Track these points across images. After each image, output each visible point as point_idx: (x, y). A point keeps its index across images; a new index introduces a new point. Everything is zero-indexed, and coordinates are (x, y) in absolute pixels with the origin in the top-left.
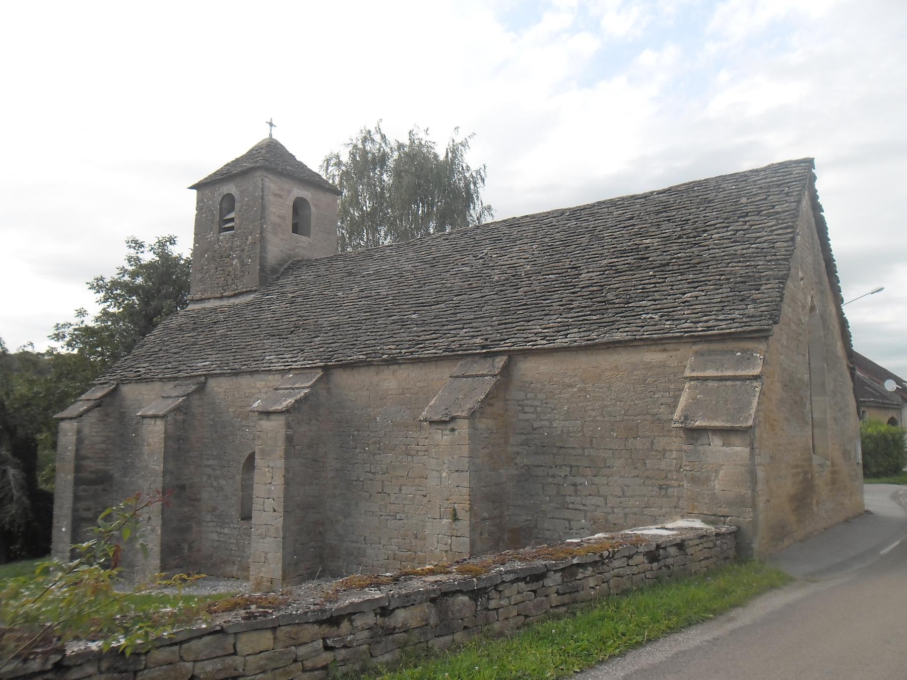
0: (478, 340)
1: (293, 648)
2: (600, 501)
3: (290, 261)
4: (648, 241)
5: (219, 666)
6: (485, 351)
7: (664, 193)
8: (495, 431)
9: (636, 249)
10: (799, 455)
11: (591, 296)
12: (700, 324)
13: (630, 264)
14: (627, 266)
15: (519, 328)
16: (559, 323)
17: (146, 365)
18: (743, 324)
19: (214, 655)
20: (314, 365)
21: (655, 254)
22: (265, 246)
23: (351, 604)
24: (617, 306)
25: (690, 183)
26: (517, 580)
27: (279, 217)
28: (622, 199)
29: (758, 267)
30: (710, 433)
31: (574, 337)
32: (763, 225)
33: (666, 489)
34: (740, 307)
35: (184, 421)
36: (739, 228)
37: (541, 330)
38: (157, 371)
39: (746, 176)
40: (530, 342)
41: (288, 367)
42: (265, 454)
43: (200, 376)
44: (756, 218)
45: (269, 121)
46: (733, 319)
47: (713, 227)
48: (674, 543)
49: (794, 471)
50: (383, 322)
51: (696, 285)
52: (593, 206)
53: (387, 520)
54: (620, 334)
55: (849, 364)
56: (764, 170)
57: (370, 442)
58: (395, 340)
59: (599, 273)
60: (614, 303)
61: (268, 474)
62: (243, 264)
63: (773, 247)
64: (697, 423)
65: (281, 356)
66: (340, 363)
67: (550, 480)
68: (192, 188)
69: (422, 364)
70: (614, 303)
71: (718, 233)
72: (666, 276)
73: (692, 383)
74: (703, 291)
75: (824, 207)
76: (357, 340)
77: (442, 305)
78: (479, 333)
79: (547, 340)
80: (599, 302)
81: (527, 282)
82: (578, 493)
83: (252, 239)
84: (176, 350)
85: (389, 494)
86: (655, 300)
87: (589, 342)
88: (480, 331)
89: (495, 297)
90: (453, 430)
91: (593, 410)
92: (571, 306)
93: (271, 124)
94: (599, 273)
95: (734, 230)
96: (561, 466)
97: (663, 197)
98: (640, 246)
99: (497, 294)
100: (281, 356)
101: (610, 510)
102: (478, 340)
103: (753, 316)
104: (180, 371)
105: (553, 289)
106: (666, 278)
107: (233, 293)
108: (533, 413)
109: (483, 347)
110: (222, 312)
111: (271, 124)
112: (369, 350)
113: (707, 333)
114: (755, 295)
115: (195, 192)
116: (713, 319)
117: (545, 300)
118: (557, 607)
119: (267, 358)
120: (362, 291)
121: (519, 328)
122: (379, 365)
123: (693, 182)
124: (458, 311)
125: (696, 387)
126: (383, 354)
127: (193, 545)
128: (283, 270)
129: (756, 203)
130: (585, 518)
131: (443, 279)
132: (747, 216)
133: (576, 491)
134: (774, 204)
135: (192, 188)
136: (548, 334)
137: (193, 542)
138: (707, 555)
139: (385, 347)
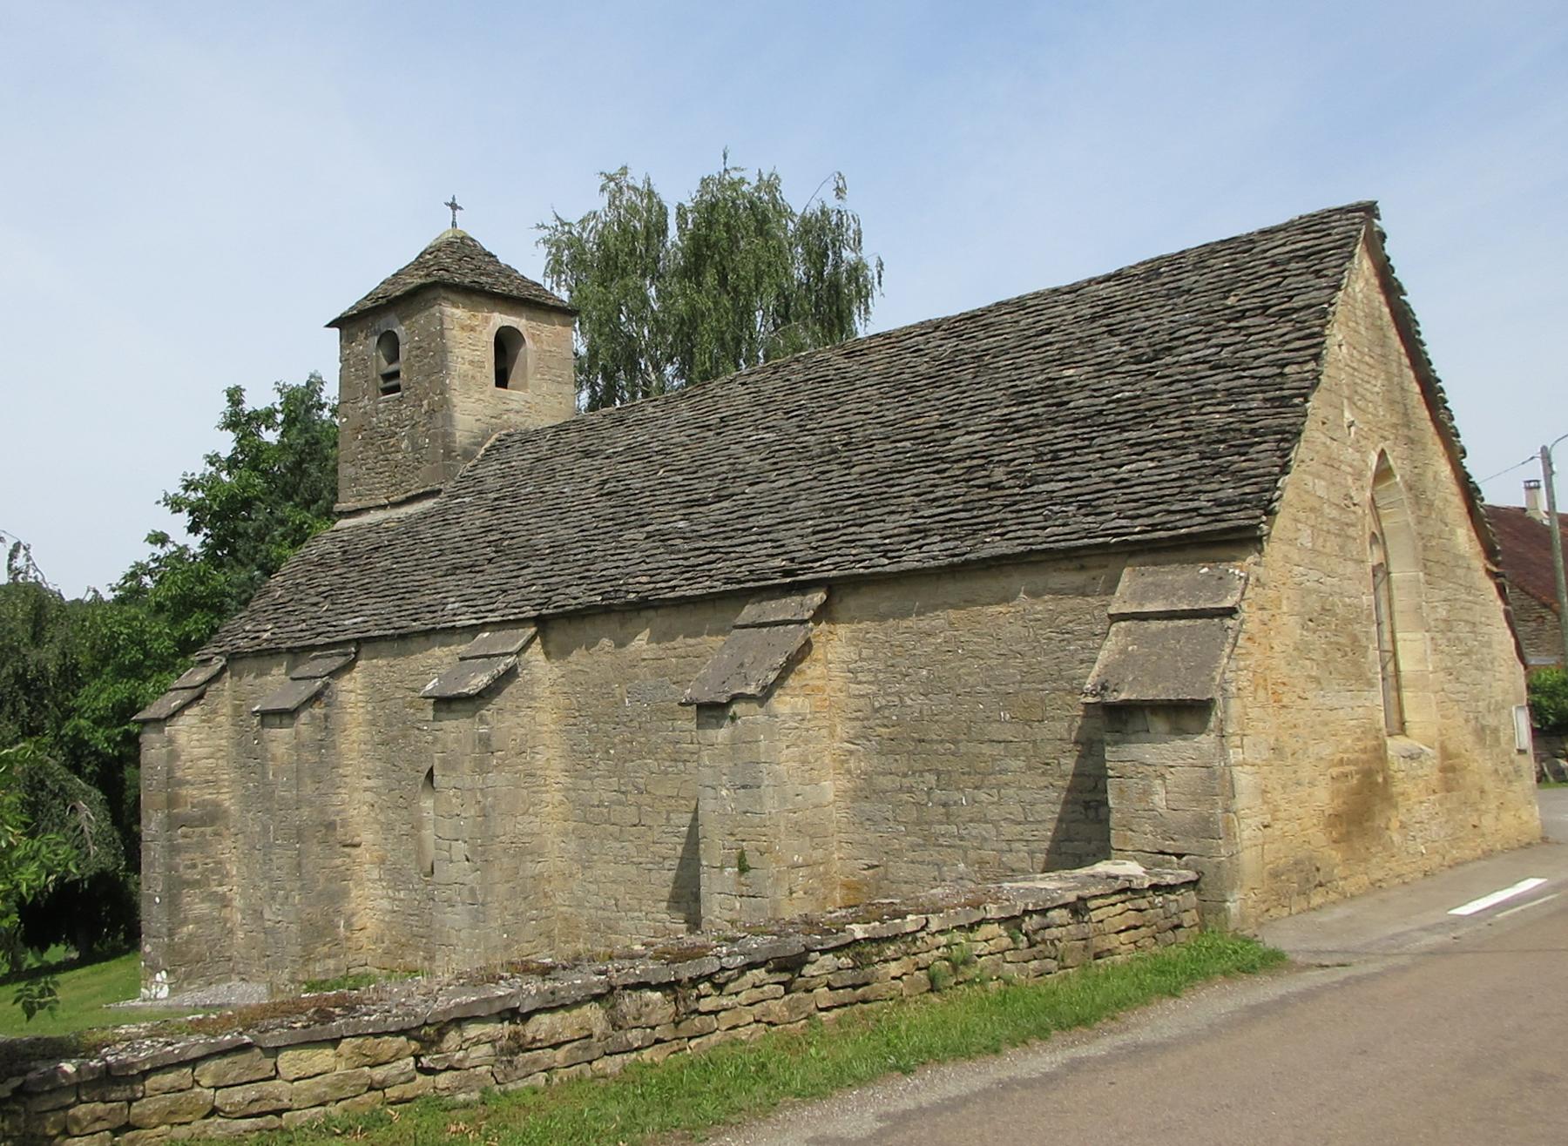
0: (777, 562)
1: (366, 1069)
2: (987, 830)
3: (496, 436)
4: (1071, 372)
5: (253, 1094)
6: (788, 580)
7: (1109, 280)
8: (809, 716)
9: (1049, 388)
10: (1349, 741)
11: (966, 477)
12: (1140, 521)
13: (1037, 415)
14: (1031, 419)
15: (844, 538)
16: (909, 526)
17: (269, 627)
18: (1210, 518)
19: (245, 1080)
20: (521, 616)
21: (1081, 395)
22: (451, 416)
23: (457, 1005)
24: (1008, 492)
25: (1153, 261)
26: (751, 966)
27: (471, 362)
28: (1037, 295)
29: (1249, 413)
30: (1147, 712)
31: (936, 551)
32: (1268, 334)
33: (1096, 809)
34: (1208, 487)
35: (326, 717)
36: (1227, 341)
37: (879, 542)
38: (284, 636)
39: (1251, 241)
40: (860, 562)
41: (481, 621)
42: (448, 765)
43: (348, 642)
44: (1257, 320)
45: (450, 201)
46: (1195, 510)
47: (1182, 342)
48: (1060, 902)
49: (1335, 771)
50: (632, 536)
51: (1142, 449)
52: (989, 310)
53: (650, 870)
54: (1005, 543)
55: (1489, 566)
56: (1284, 230)
57: (616, 741)
58: (650, 566)
59: (983, 434)
60: (1003, 488)
61: (454, 800)
62: (416, 448)
63: (1281, 374)
64: (1123, 696)
65: (470, 603)
66: (560, 610)
67: (905, 797)
68: (329, 325)
69: (691, 606)
70: (1003, 488)
71: (1191, 352)
72: (1094, 434)
73: (1123, 624)
74: (1152, 460)
75: (1406, 288)
76: (588, 570)
77: (725, 504)
78: (779, 551)
79: (889, 558)
80: (979, 487)
81: (866, 456)
82: (952, 818)
83: (429, 404)
84: (315, 600)
85: (650, 827)
86: (1071, 480)
87: (955, 559)
88: (783, 546)
89: (814, 483)
90: (733, 719)
91: (969, 674)
92: (932, 496)
93: (454, 206)
94: (983, 434)
95: (1216, 346)
96: (921, 772)
97: (1104, 291)
98: (1058, 382)
99: (815, 478)
100: (470, 603)
101: (1005, 846)
102: (777, 562)
103: (1229, 503)
104: (319, 634)
105: (907, 467)
106: (1094, 438)
107: (403, 497)
108: (870, 683)
109: (787, 573)
110: (387, 530)
111: (454, 206)
112: (607, 586)
113: (1148, 536)
114: (1240, 463)
115: (337, 330)
116: (1159, 512)
117: (893, 486)
118: (827, 1009)
119: (450, 606)
120: (605, 482)
121: (844, 538)
122: (623, 612)
123: (1158, 259)
124: (753, 512)
125: (1128, 632)
126: (628, 592)
127: (354, 919)
128: (483, 452)
129: (1259, 294)
130: (965, 859)
131: (730, 456)
132: (1243, 317)
133: (947, 815)
134: (1291, 293)
135: (329, 325)
136: (890, 547)
137: (353, 915)
138: (1132, 922)
139: (631, 581)
